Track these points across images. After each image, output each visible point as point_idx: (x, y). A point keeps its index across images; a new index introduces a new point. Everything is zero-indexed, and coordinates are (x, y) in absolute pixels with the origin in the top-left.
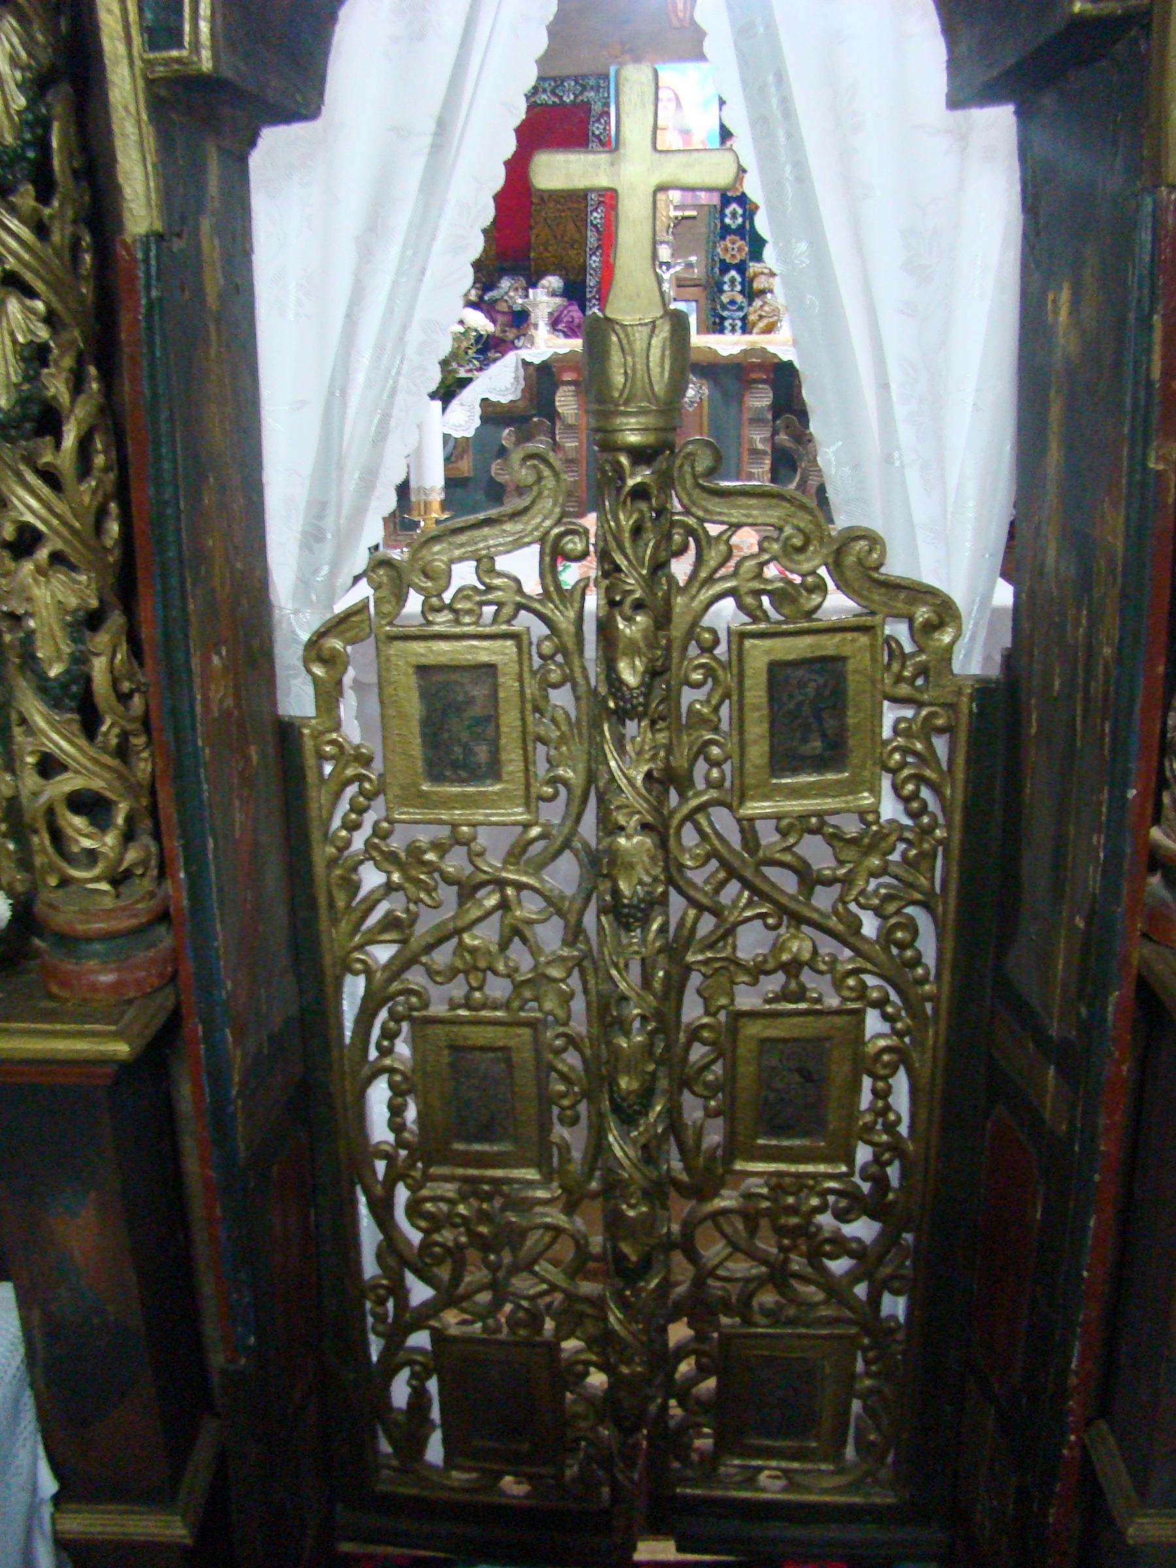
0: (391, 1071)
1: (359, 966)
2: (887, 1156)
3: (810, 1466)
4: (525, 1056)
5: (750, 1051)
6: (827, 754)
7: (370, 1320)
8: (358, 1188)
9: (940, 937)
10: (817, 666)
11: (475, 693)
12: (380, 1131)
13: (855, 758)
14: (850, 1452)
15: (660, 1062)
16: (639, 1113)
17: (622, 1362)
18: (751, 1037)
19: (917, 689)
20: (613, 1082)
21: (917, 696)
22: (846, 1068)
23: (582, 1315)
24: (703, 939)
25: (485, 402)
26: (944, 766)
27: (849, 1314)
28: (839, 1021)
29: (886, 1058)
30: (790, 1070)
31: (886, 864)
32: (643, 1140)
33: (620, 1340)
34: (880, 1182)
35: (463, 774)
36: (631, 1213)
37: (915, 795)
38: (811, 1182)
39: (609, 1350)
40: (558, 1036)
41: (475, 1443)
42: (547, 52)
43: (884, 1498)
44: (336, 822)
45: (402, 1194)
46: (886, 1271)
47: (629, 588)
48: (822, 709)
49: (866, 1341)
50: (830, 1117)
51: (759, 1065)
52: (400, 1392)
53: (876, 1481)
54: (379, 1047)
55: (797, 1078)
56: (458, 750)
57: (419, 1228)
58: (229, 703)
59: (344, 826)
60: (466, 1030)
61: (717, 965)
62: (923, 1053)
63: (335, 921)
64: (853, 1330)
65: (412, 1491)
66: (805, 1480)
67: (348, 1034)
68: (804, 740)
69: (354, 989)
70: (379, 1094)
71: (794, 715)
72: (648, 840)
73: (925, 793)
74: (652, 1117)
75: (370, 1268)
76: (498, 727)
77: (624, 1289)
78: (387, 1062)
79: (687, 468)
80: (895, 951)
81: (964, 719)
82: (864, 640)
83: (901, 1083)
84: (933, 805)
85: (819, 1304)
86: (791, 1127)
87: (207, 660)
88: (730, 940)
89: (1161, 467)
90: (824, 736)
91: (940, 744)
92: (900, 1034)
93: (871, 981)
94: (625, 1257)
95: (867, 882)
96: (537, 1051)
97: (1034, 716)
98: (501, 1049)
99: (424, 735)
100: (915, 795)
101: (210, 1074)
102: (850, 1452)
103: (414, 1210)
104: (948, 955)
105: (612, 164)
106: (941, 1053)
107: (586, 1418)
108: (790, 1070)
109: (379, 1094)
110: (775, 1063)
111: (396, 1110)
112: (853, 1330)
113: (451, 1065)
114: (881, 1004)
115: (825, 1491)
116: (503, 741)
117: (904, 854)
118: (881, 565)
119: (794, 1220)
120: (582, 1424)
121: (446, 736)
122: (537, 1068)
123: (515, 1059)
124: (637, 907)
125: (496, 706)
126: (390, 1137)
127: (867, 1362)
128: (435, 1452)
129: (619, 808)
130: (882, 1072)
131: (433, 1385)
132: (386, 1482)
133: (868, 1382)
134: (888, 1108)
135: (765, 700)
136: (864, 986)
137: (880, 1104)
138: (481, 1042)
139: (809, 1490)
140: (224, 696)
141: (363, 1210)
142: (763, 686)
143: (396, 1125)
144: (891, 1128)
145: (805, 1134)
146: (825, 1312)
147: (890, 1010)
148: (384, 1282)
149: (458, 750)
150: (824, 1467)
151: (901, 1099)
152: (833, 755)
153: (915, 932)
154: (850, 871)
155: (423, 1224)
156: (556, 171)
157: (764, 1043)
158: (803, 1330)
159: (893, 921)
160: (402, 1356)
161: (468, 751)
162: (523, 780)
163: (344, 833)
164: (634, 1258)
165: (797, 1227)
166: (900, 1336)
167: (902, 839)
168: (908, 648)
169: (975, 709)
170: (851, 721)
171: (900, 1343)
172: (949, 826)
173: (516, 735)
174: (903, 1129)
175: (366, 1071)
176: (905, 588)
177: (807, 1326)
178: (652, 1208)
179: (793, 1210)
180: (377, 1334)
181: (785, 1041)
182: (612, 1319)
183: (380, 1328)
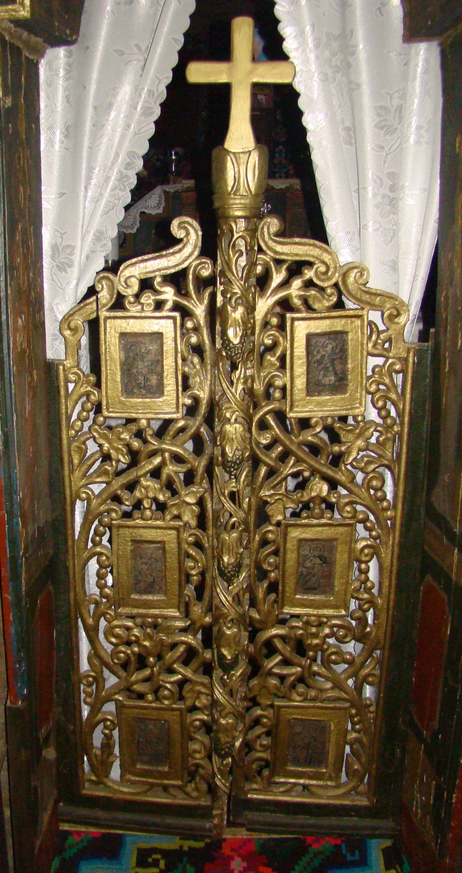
0: (100, 554)
1: (84, 495)
2: (366, 606)
3: (321, 783)
4: (172, 546)
5: (293, 546)
6: (337, 383)
7: (83, 695)
8: (80, 620)
9: (396, 484)
10: (332, 336)
11: (151, 348)
12: (92, 588)
13: (351, 386)
14: (344, 777)
15: (246, 548)
16: (234, 576)
17: (221, 716)
18: (294, 537)
19: (385, 350)
20: (220, 558)
21: (385, 353)
22: (346, 556)
23: (200, 693)
24: (214, 586)
25: (143, 213)
26: (400, 391)
27: (344, 695)
28: (341, 529)
29: (366, 551)
30: (314, 556)
31: (368, 444)
32: (236, 591)
33: (222, 705)
34: (362, 621)
35: (144, 392)
36: (228, 632)
37: (384, 407)
38: (325, 620)
39: (214, 711)
40: (190, 535)
41: (138, 766)
42: (195, 11)
43: (363, 802)
44: (74, 417)
45: (103, 623)
46: (365, 672)
47: (235, 291)
48: (334, 360)
49: (354, 711)
50: (336, 583)
51: (299, 554)
52: (98, 738)
53: (357, 793)
54: (93, 541)
55: (319, 561)
56: (141, 378)
57: (111, 643)
58: (25, 345)
59: (79, 418)
60: (142, 531)
61: (277, 498)
62: (387, 549)
63: (71, 471)
64: (347, 705)
65: (102, 794)
66: (319, 792)
67: (77, 534)
68: (325, 376)
69: (79, 508)
70: (93, 566)
71: (319, 362)
72: (278, 364)
73: (389, 405)
74: (241, 578)
75: (85, 666)
76: (162, 366)
77: (224, 675)
78: (98, 549)
79: (265, 230)
80: (372, 492)
81: (410, 366)
82: (358, 322)
83: (373, 565)
84: (393, 413)
85: (328, 689)
86: (315, 589)
87: (16, 322)
88: (284, 484)
90: (336, 374)
91: (399, 379)
92: (375, 539)
93: (359, 508)
94: (224, 657)
95: (358, 454)
96: (179, 543)
97: (447, 362)
98: (159, 542)
99: (122, 370)
100: (384, 407)
101: (10, 542)
102: (344, 777)
103: (109, 632)
104: (401, 494)
105: (230, 69)
106: (396, 549)
107: (199, 752)
108: (314, 556)
109: (93, 566)
110: (306, 552)
111: (100, 576)
112: (347, 705)
113: (132, 551)
114: (364, 521)
115: (329, 797)
116: (165, 374)
117: (377, 439)
118: (368, 282)
119: (316, 641)
120: (198, 756)
121: (135, 371)
122: (179, 555)
123: (167, 547)
124: (235, 463)
125: (162, 355)
126: (97, 591)
127: (353, 724)
128: (115, 773)
129: (227, 409)
130: (364, 559)
131: (116, 733)
132: (88, 790)
133: (354, 735)
134: (367, 579)
135: (305, 353)
136: (355, 511)
137: (363, 576)
138: (149, 538)
139: (320, 797)
140: (23, 340)
141: (83, 634)
142: (304, 346)
143: (101, 587)
144: (368, 590)
145: (323, 592)
146: (330, 694)
147: (369, 524)
148: (92, 674)
149: (141, 378)
150: (329, 783)
151: (373, 575)
152: (340, 385)
153: (383, 482)
154: (349, 447)
155: (114, 640)
156: (200, 73)
157: (301, 541)
158: (320, 704)
159: (371, 475)
160: (100, 716)
161: (147, 380)
162: (175, 395)
163: (79, 423)
164: (229, 657)
165: (317, 645)
166: (372, 709)
167: (376, 430)
168: (382, 327)
169: (416, 361)
170: (350, 366)
171: (372, 713)
172: (402, 424)
173: (172, 370)
174: (375, 591)
175: (86, 555)
176: (379, 295)
177: (322, 702)
178: (239, 630)
179: (315, 636)
180: (86, 703)
181: (312, 540)
182: (216, 692)
183: (89, 700)
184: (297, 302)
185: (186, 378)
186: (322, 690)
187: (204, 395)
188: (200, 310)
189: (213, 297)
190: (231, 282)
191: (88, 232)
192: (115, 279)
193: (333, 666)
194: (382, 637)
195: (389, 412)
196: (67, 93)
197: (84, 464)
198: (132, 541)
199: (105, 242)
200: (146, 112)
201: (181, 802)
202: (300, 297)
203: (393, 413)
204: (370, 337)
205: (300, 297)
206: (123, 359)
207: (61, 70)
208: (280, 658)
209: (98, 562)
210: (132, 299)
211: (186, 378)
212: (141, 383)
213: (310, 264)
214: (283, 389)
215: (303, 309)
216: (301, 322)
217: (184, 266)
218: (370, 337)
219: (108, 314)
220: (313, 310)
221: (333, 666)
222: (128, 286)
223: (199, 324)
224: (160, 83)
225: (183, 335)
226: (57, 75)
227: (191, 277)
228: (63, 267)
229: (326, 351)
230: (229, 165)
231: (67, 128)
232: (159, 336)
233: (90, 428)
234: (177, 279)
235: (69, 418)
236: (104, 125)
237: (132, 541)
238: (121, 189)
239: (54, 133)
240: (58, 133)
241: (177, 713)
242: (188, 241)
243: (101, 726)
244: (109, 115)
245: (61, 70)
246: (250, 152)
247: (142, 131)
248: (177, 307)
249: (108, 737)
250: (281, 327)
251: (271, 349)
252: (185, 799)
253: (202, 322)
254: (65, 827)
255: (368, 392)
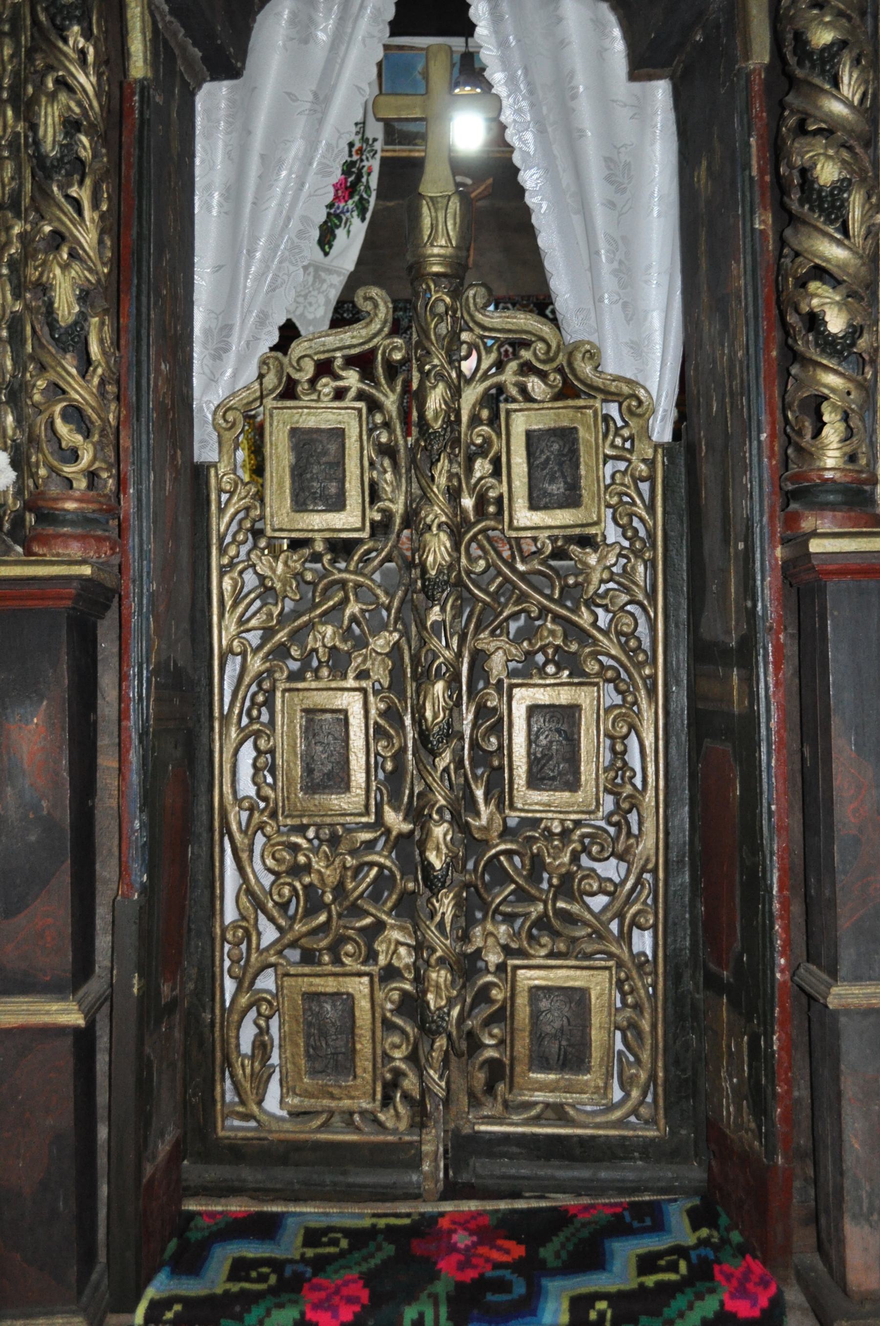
7: (227, 963)
57: (270, 870)
63: (221, 616)
75: (230, 914)
76: (344, 470)
84: (642, 533)
89: (762, 227)
94: (430, 865)
99: (293, 476)
126: (251, 791)
131: (274, 1023)
152: (572, 500)
184: (514, 392)
185: (373, 485)
186: (574, 940)
187: (398, 508)
188: (390, 401)
189: (407, 383)
190: (431, 789)
191: (249, 311)
192: (286, 360)
193: (587, 899)
194: (652, 852)
195: (636, 531)
196: (230, 148)
197: (240, 603)
198: (303, 710)
199: (270, 328)
200: (324, 171)
201: (373, 1138)
202: (516, 384)
203: (642, 533)
204: (605, 436)
205: (516, 384)
206: (293, 461)
207: (222, 123)
208: (513, 886)
209: (256, 747)
210: (306, 386)
211: (373, 485)
212: (315, 493)
213: (527, 344)
214: (499, 500)
215: (521, 399)
216: (519, 414)
217: (371, 345)
218: (605, 436)
219: (275, 404)
220: (534, 401)
221: (587, 899)
222: (300, 370)
223: (391, 417)
224: (340, 137)
225: (370, 431)
226: (217, 128)
227: (379, 357)
228: (219, 354)
229: (552, 452)
230: (425, 210)
231: (228, 189)
232: (339, 434)
233: (249, 553)
234: (362, 362)
235: (221, 539)
236: (271, 186)
237: (303, 710)
238: (291, 263)
239: (211, 196)
240: (216, 195)
241: (366, 980)
242: (376, 315)
243: (253, 1014)
244: (278, 174)
245: (222, 123)
246: (449, 197)
247: (319, 192)
248: (361, 396)
249: (263, 1031)
250: (493, 421)
251: (483, 451)
252: (377, 1134)
253: (394, 414)
254: (192, 1206)
255: (608, 506)
